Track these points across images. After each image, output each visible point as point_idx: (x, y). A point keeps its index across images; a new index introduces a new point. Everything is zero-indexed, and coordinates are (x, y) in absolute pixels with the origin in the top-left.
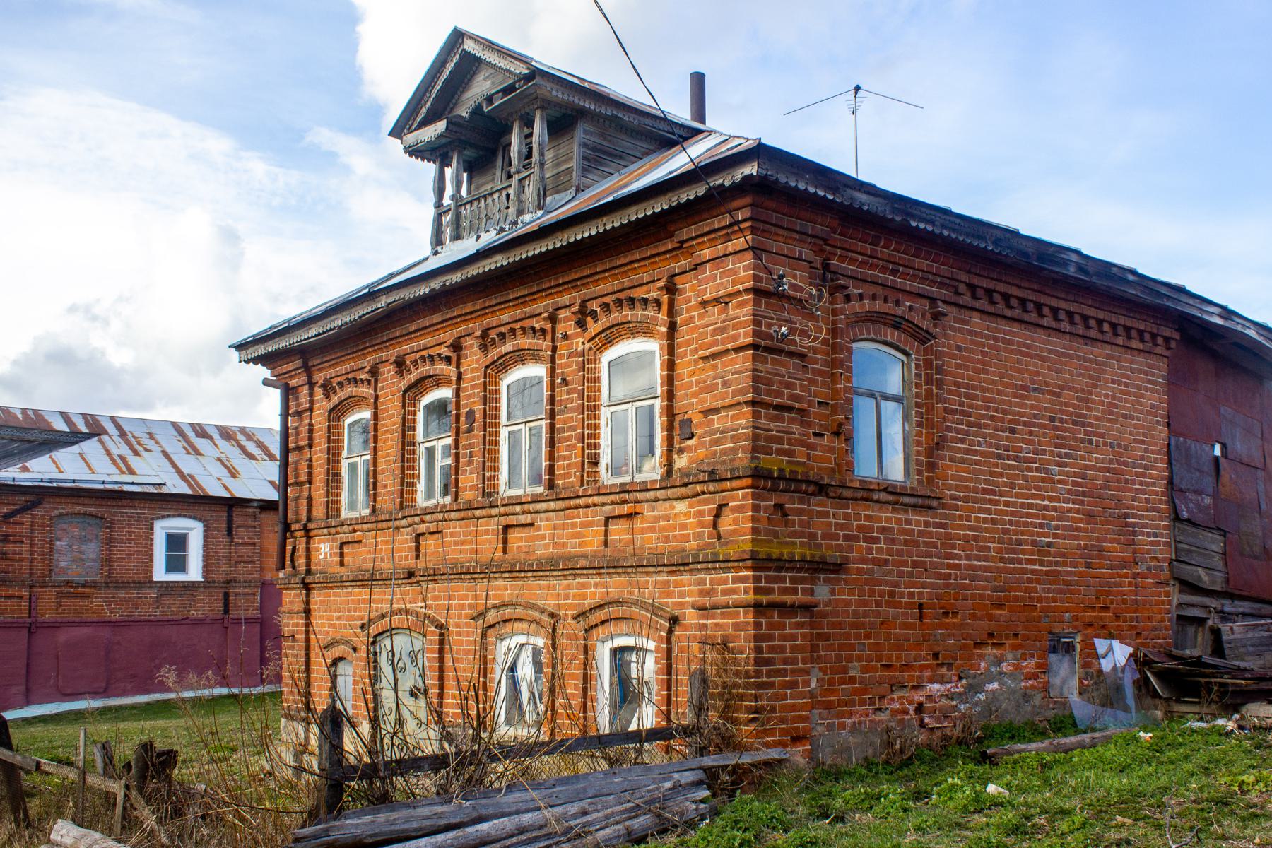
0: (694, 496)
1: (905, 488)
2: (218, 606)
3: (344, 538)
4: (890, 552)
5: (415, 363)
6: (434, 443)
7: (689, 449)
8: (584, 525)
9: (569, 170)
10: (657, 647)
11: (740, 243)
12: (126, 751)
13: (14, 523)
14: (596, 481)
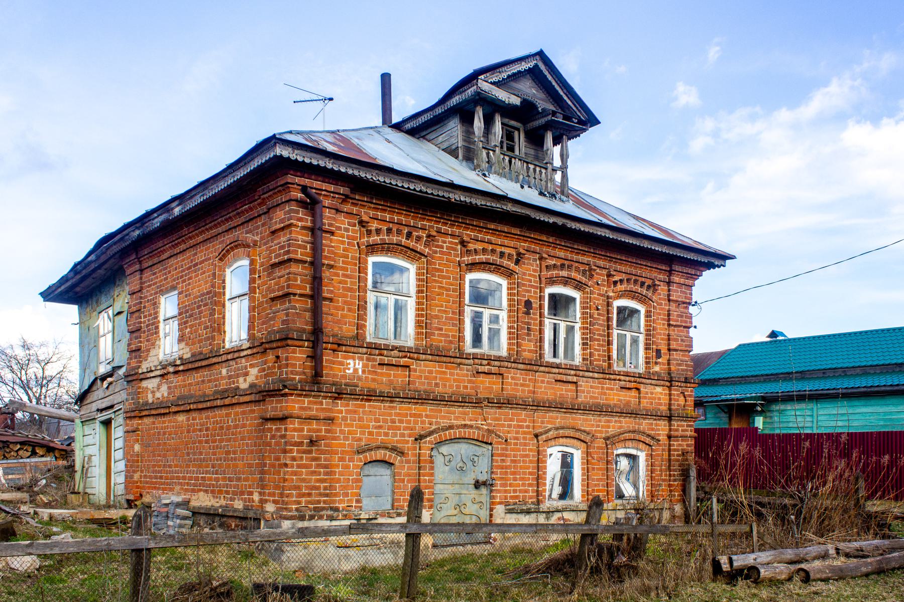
8: (608, 389)
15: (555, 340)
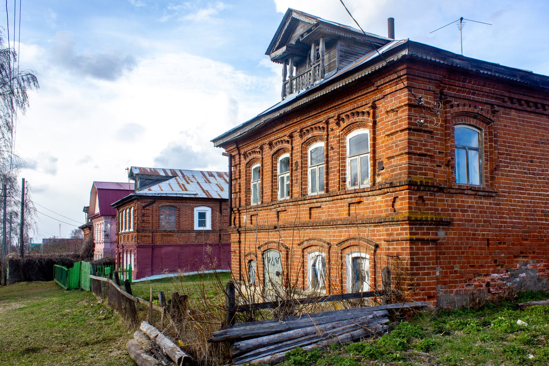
0: (384, 194)
1: (480, 188)
2: (217, 239)
3: (252, 213)
4: (473, 216)
5: (276, 144)
6: (283, 175)
7: (382, 174)
8: (340, 207)
9: (334, 62)
10: (370, 257)
11: (401, 85)
12: (169, 296)
13: (147, 209)
14: (345, 189)
15: (80, 274)
